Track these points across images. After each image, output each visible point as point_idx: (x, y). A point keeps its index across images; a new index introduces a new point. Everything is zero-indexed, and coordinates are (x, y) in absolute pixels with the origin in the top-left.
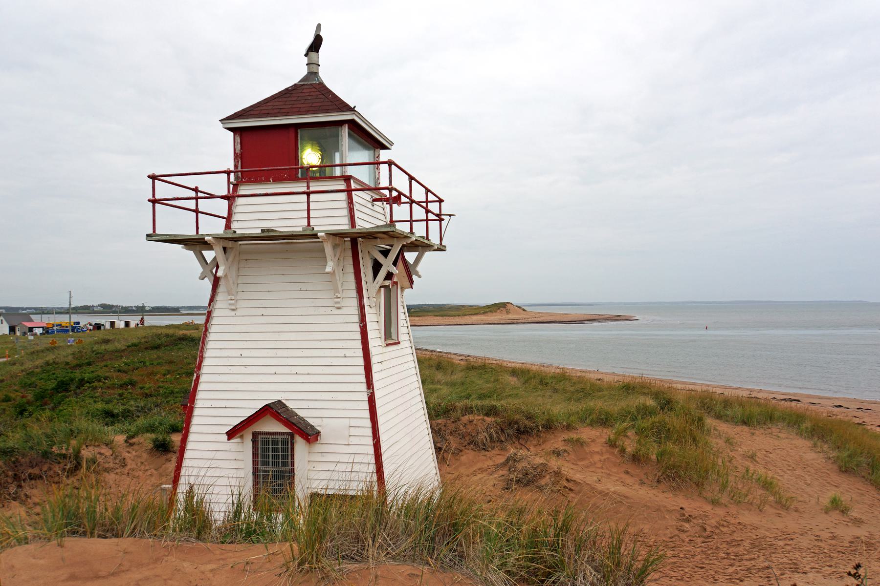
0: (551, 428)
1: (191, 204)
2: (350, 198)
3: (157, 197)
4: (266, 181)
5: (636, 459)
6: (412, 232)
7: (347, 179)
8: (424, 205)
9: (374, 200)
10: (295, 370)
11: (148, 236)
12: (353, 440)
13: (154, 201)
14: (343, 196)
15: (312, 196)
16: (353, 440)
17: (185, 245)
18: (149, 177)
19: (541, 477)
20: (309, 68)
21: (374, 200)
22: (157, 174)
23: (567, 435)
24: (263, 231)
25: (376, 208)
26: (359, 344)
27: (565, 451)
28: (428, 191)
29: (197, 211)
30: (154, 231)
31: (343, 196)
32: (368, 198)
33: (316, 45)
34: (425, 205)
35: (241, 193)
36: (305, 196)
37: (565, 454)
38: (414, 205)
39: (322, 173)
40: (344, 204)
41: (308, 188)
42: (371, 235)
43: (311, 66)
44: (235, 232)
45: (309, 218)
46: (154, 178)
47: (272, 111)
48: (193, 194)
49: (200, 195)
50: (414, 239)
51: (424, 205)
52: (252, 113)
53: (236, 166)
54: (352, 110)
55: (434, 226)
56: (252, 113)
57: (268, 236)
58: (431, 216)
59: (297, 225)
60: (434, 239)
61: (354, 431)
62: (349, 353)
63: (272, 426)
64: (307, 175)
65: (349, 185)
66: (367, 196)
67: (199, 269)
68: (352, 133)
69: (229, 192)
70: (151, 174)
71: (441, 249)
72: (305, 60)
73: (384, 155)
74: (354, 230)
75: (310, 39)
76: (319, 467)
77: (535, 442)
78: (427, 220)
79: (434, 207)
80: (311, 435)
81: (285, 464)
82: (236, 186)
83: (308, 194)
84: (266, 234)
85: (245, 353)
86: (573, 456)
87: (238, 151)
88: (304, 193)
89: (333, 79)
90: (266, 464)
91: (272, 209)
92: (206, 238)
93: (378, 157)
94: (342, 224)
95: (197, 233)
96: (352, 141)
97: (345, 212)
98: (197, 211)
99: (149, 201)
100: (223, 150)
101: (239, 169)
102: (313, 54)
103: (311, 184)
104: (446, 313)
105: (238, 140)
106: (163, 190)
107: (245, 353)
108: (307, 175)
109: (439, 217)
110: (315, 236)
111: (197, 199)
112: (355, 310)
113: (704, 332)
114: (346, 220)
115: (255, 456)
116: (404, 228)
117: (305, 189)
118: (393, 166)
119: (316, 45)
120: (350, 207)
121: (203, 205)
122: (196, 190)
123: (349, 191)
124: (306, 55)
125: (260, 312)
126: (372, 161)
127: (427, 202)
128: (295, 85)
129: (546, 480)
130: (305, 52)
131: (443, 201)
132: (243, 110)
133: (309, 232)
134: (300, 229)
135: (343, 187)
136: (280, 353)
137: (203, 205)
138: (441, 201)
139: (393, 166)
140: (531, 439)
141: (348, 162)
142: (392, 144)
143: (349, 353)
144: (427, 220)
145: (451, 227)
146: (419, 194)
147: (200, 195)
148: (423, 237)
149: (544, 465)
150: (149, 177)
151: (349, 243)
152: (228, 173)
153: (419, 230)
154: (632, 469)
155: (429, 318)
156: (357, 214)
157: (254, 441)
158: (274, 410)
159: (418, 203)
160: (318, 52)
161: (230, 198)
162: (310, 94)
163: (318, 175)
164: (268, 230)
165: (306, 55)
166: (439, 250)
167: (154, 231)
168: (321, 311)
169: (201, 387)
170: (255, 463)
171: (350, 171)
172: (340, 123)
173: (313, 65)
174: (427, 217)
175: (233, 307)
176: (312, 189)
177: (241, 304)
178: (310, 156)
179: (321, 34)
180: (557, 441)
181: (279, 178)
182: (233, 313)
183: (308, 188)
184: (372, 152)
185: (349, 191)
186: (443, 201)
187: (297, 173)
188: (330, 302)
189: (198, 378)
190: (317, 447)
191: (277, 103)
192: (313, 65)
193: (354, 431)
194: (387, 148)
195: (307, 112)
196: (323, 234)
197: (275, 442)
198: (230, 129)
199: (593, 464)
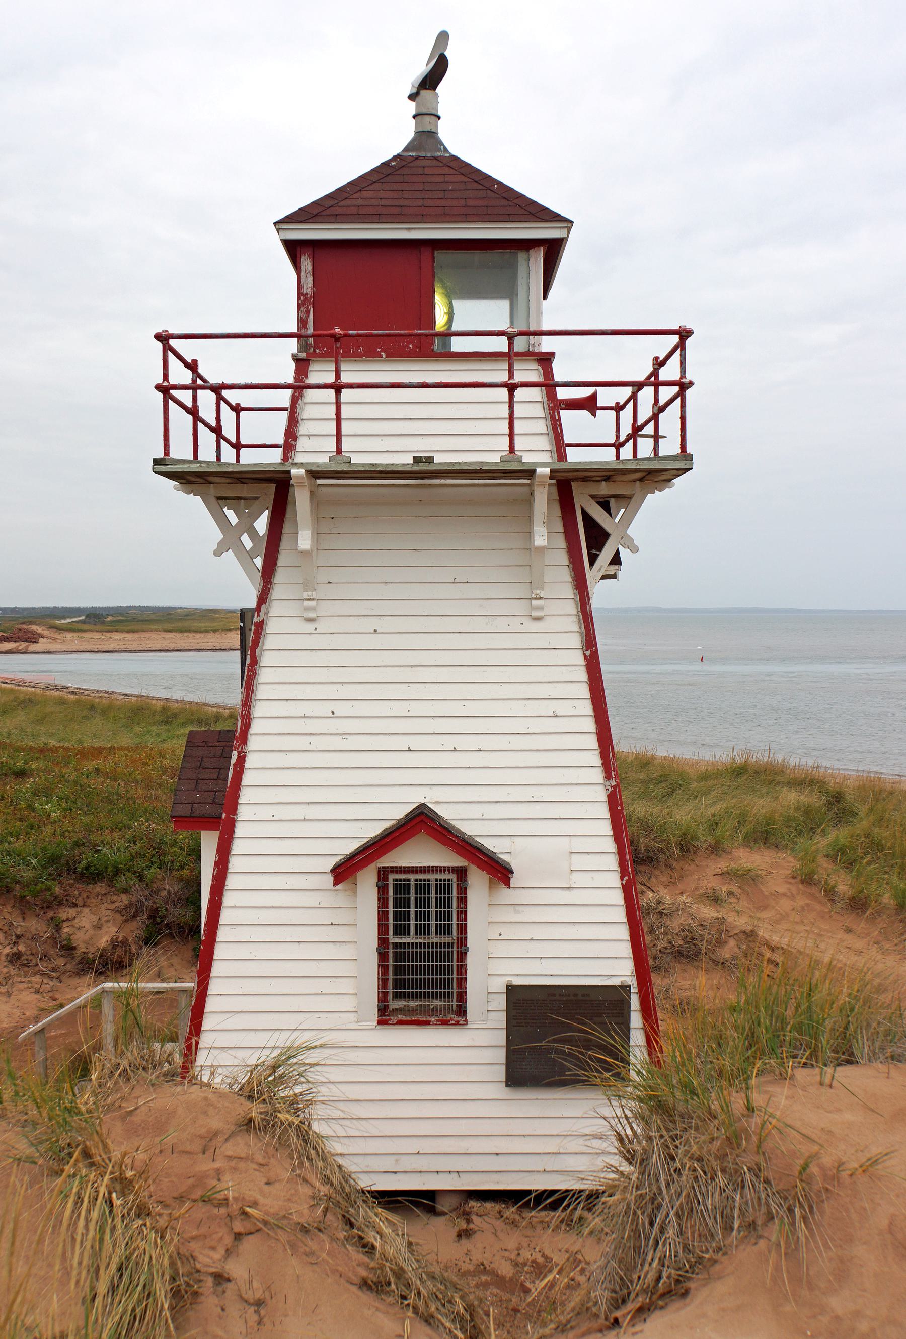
0: (688, 851)
5: (858, 904)
10: (450, 742)
11: (156, 462)
12: (579, 879)
15: (344, 392)
16: (579, 879)
19: (720, 943)
23: (723, 864)
24: (417, 460)
26: (584, 691)
27: (730, 893)
30: (167, 453)
33: (432, 79)
36: (504, 392)
37: (733, 900)
41: (511, 376)
53: (302, 323)
57: (423, 471)
59: (491, 453)
61: (578, 862)
62: (563, 708)
63: (420, 855)
65: (548, 372)
67: (218, 535)
72: (411, 107)
75: (421, 67)
76: (508, 932)
77: (664, 879)
80: (500, 872)
81: (444, 930)
83: (338, 388)
85: (341, 709)
86: (744, 903)
89: (459, 139)
90: (402, 930)
91: (392, 416)
95: (238, 461)
100: (276, 293)
101: (311, 331)
103: (343, 367)
104: (186, 624)
107: (341, 709)
112: (572, 624)
113: (698, 667)
115: (382, 916)
117: (503, 377)
119: (432, 79)
124: (412, 97)
125: (374, 624)
129: (728, 950)
130: (408, 90)
133: (514, 466)
136: (417, 709)
140: (657, 872)
141: (545, 327)
143: (563, 708)
149: (721, 921)
154: (849, 920)
155: (153, 635)
157: (382, 888)
158: (422, 822)
160: (435, 89)
162: (424, 176)
165: (412, 97)
167: (167, 453)
168: (501, 624)
169: (248, 778)
170: (382, 929)
173: (426, 117)
175: (312, 615)
176: (519, 378)
177: (325, 608)
179: (446, 54)
180: (707, 873)
182: (310, 627)
183: (511, 376)
188: (519, 608)
189: (242, 759)
190: (505, 895)
192: (426, 117)
193: (578, 862)
195: (465, 217)
197: (422, 887)
199: (784, 917)
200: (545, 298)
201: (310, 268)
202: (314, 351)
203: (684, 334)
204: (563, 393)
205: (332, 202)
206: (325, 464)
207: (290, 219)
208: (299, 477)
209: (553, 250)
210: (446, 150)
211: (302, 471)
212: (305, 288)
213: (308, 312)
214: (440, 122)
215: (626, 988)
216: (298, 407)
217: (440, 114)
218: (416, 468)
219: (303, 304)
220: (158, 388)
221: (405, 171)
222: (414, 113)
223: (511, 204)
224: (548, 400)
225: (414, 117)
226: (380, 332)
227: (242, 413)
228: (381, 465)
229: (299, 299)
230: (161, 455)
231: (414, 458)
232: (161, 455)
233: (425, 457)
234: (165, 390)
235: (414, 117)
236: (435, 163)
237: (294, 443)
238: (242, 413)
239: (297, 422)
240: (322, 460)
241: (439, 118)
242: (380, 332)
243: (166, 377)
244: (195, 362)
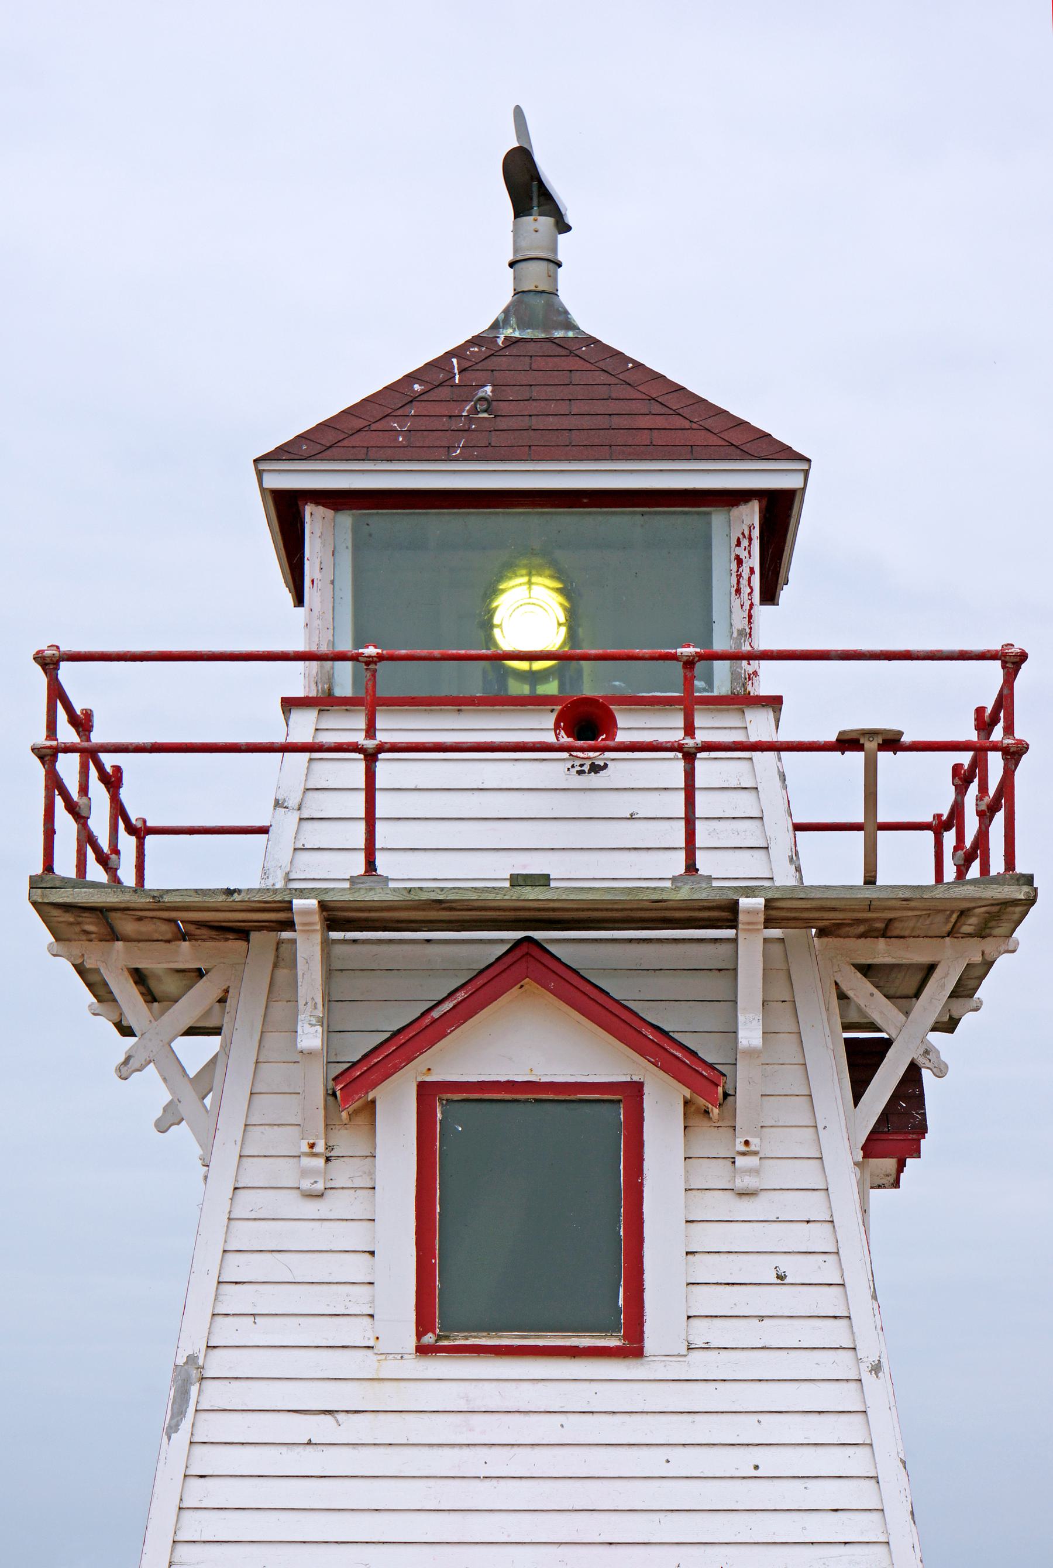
60: (945, 703)
89: (600, 304)
173: (538, 266)
176: (382, 737)
182: (312, 1209)
200: (769, 596)
203: (1013, 662)
205: (359, 423)
207: (285, 453)
208: (306, 912)
209: (779, 512)
210: (570, 325)
211: (313, 903)
214: (560, 270)
215: (712, 691)
217: (560, 257)
220: (37, 751)
222: (510, 257)
223: (694, 426)
225: (512, 265)
227: (150, 839)
234: (47, 756)
235: (512, 265)
238: (150, 839)
240: (341, 892)
241: (559, 265)
244: (88, 715)
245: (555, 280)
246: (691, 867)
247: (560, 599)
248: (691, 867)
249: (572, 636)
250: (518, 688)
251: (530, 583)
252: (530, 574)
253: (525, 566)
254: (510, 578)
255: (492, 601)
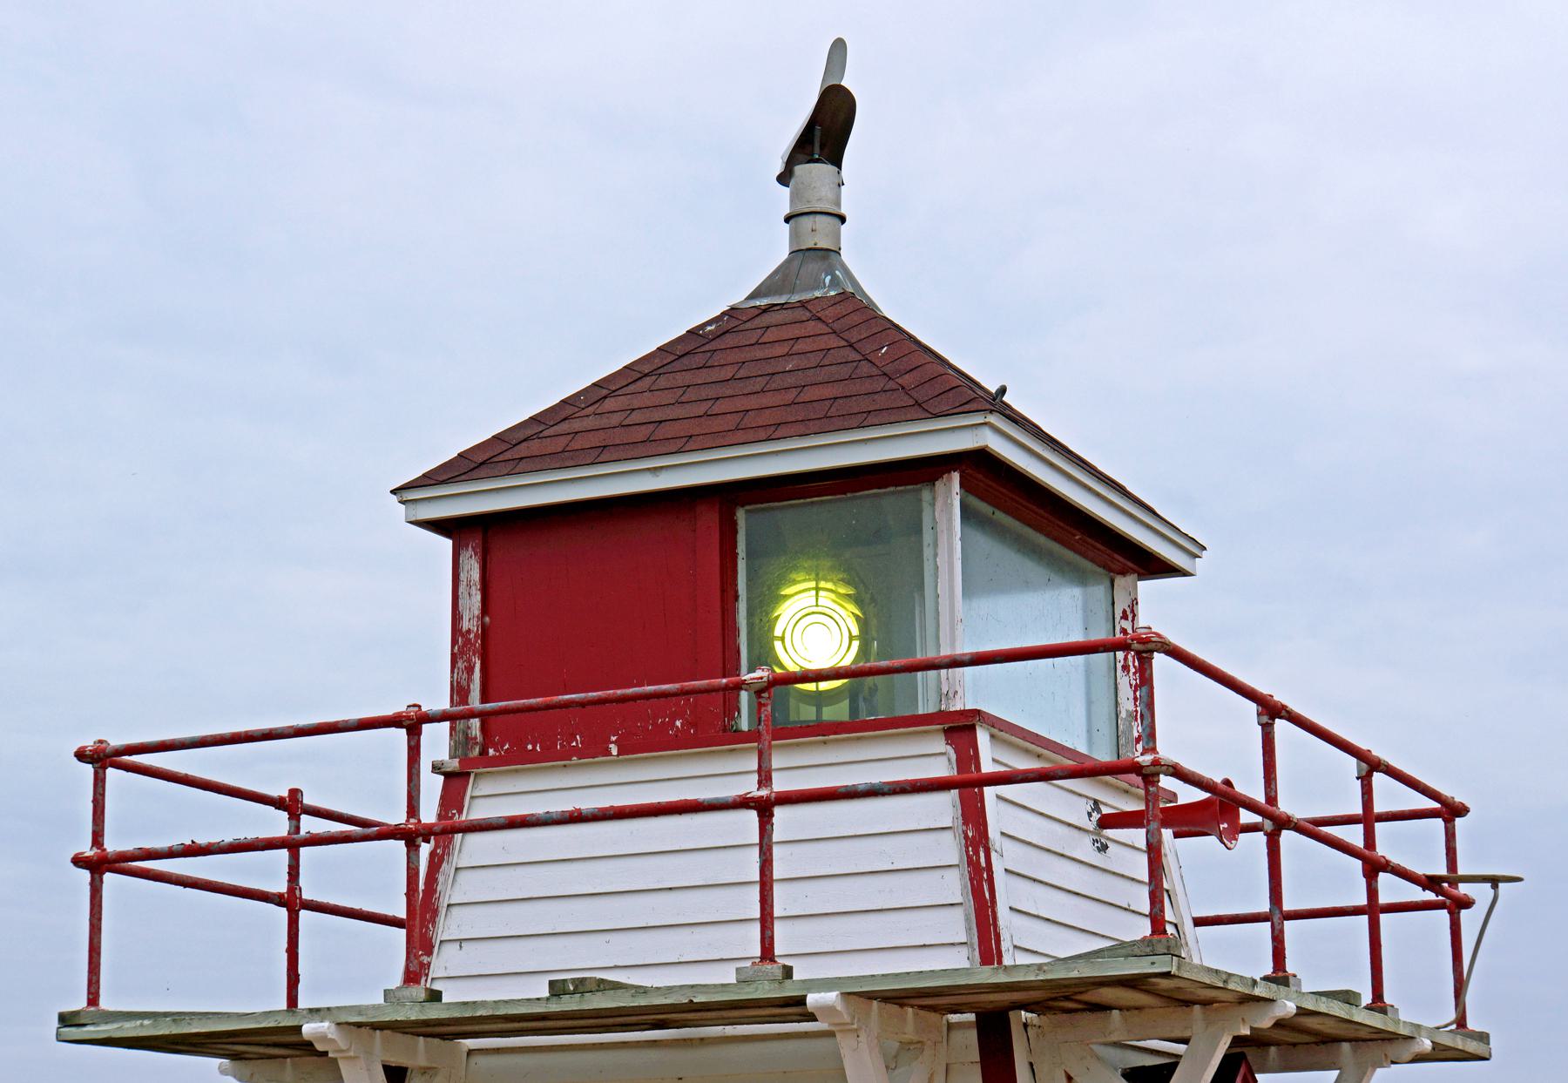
1: (270, 871)
2: (974, 815)
3: (112, 845)
4: (594, 750)
6: (1280, 976)
7: (960, 728)
8: (1353, 835)
9: (1107, 822)
11: (66, 1020)
13: (98, 865)
14: (944, 807)
15: (780, 813)
17: (235, 1057)
18: (81, 755)
20: (795, 236)
21: (1107, 822)
22: (116, 741)
24: (557, 989)
25: (1117, 858)
28: (1371, 765)
29: (292, 902)
31: (944, 807)
32: (1078, 812)
33: (827, 130)
34: (1359, 838)
35: (477, 811)
38: (1287, 837)
39: (872, 699)
40: (950, 849)
41: (765, 778)
42: (1068, 999)
43: (806, 222)
44: (435, 996)
45: (766, 919)
46: (100, 758)
47: (619, 436)
48: (277, 824)
49: (309, 825)
50: (1288, 1007)
51: (1353, 835)
52: (534, 447)
53: (459, 692)
54: (995, 402)
55: (1417, 940)
56: (534, 447)
58: (1391, 889)
59: (714, 960)
60: (1419, 1001)
64: (788, 713)
66: (1068, 803)
68: (975, 502)
69: (413, 810)
70: (89, 742)
71: (1458, 1045)
73: (1156, 605)
74: (987, 975)
78: (1373, 910)
79: (1414, 846)
82: (455, 782)
83: (764, 809)
84: (569, 1004)
87: (470, 623)
88: (743, 803)
89: (896, 276)
92: (309, 1029)
93: (1131, 613)
94: (943, 952)
96: (984, 543)
97: (954, 886)
98: (292, 902)
99: (78, 861)
100: (403, 619)
101: (475, 702)
102: (814, 173)
103: (777, 761)
105: (472, 569)
106: (142, 813)
108: (788, 713)
109: (1445, 893)
110: (795, 1007)
111: (292, 845)
114: (958, 925)
116: (1238, 956)
117: (749, 786)
118: (1159, 660)
119: (827, 130)
120: (973, 864)
121: (323, 873)
122: (292, 805)
123: (969, 785)
126: (1100, 634)
127: (1368, 819)
128: (733, 312)
130: (779, 167)
131: (1461, 811)
132: (497, 438)
134: (728, 975)
135: (942, 767)
137: (323, 873)
138: (1451, 811)
139: (1159, 660)
142: (1195, 548)
144: (1373, 910)
145: (1504, 935)
146: (1316, 783)
147: (309, 825)
148: (1348, 997)
150: (81, 755)
151: (973, 1035)
152: (413, 723)
153: (1327, 963)
156: (1007, 893)
159: (1312, 829)
160: (837, 161)
161: (430, 839)
163: (838, 712)
164: (581, 986)
165: (784, 178)
166: (1441, 1054)
167: (93, 999)
171: (973, 690)
172: (927, 470)
173: (814, 221)
174: (1372, 893)
176: (780, 784)
178: (812, 627)
181: (647, 737)
183: (765, 778)
184: (1099, 591)
185: (969, 785)
186: (1461, 811)
187: (732, 708)
191: (647, 399)
192: (814, 221)
194: (1156, 567)
196: (831, 997)
198: (439, 526)
201: (476, 575)
202: (484, 752)
204: (429, 813)
206: (376, 1007)
207: (1185, 574)
212: (466, 618)
213: (470, 670)
216: (441, 878)
217: (844, 211)
218: (554, 1007)
219: (462, 652)
221: (729, 340)
222: (787, 211)
224: (965, 823)
225: (787, 220)
226: (533, 701)
228: (484, 1004)
229: (454, 642)
230: (79, 1003)
231: (551, 983)
232: (79, 1003)
233: (573, 980)
235: (787, 220)
236: (801, 314)
237: (425, 959)
239: (435, 912)
241: (843, 219)
242: (533, 701)
243: (97, 838)
245: (837, 237)
246: (767, 953)
247: (852, 608)
248: (767, 953)
249: (864, 651)
250: (808, 714)
251: (817, 589)
252: (817, 580)
253: (808, 571)
254: (794, 582)
255: (773, 610)
